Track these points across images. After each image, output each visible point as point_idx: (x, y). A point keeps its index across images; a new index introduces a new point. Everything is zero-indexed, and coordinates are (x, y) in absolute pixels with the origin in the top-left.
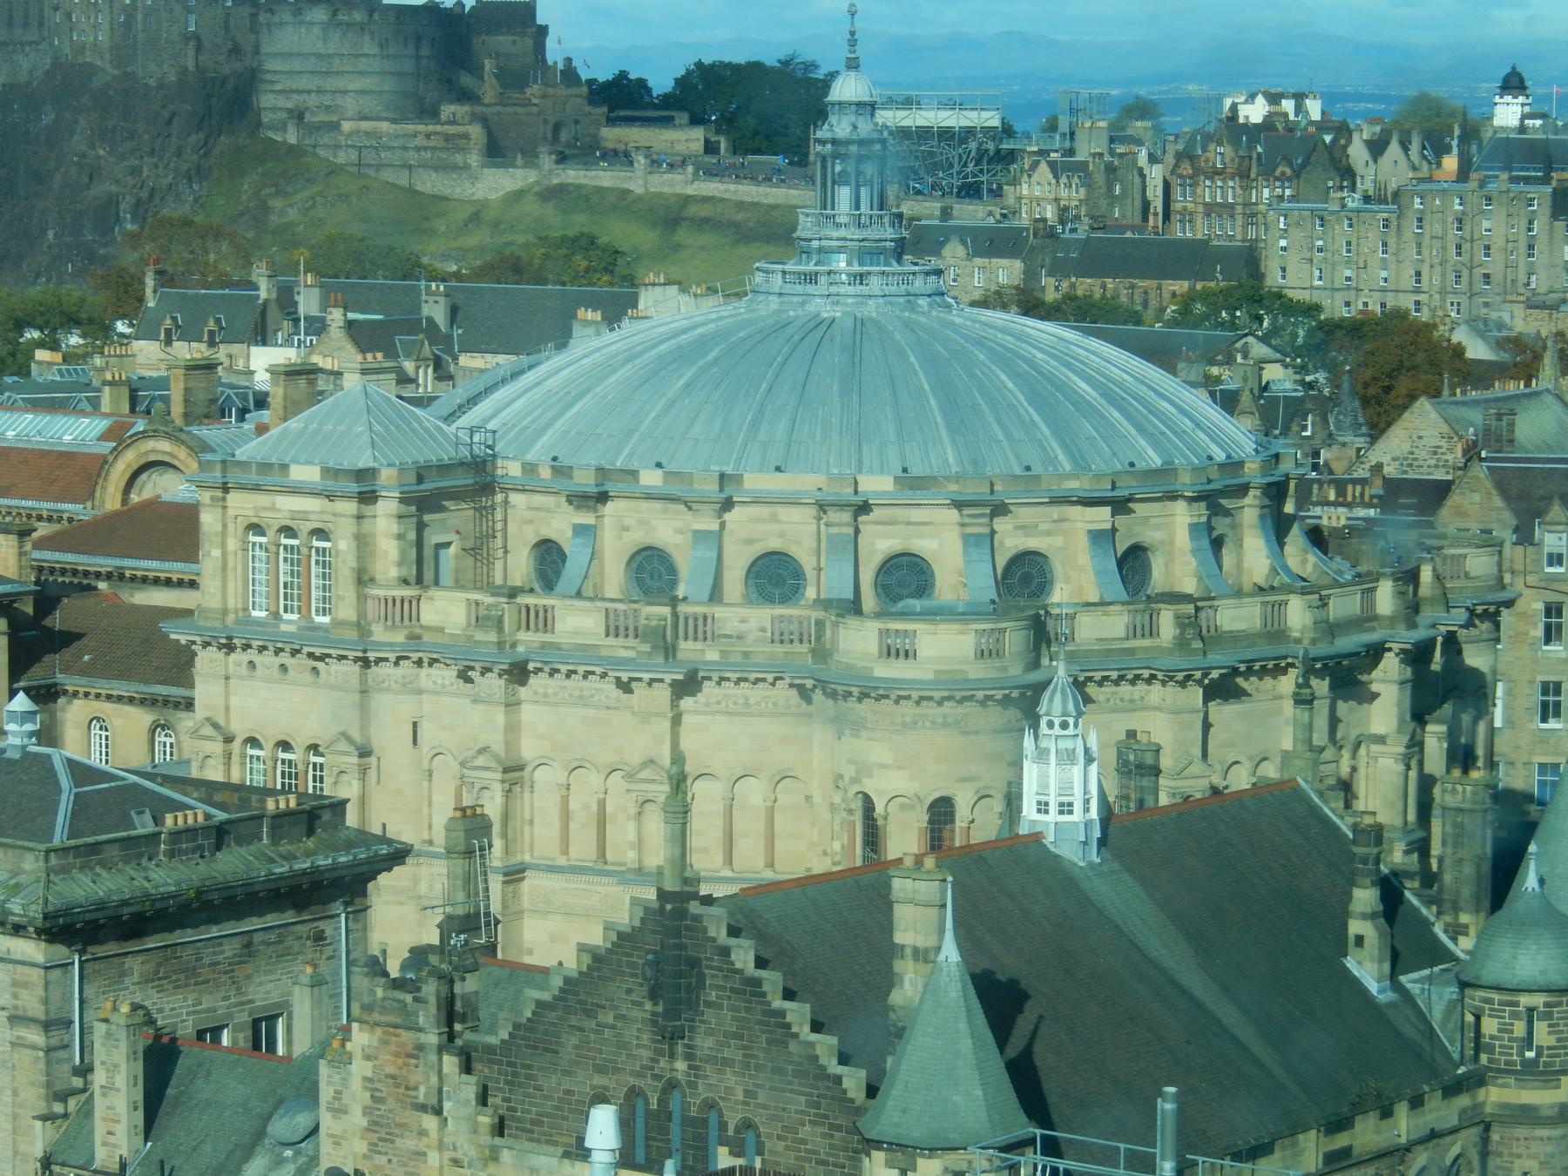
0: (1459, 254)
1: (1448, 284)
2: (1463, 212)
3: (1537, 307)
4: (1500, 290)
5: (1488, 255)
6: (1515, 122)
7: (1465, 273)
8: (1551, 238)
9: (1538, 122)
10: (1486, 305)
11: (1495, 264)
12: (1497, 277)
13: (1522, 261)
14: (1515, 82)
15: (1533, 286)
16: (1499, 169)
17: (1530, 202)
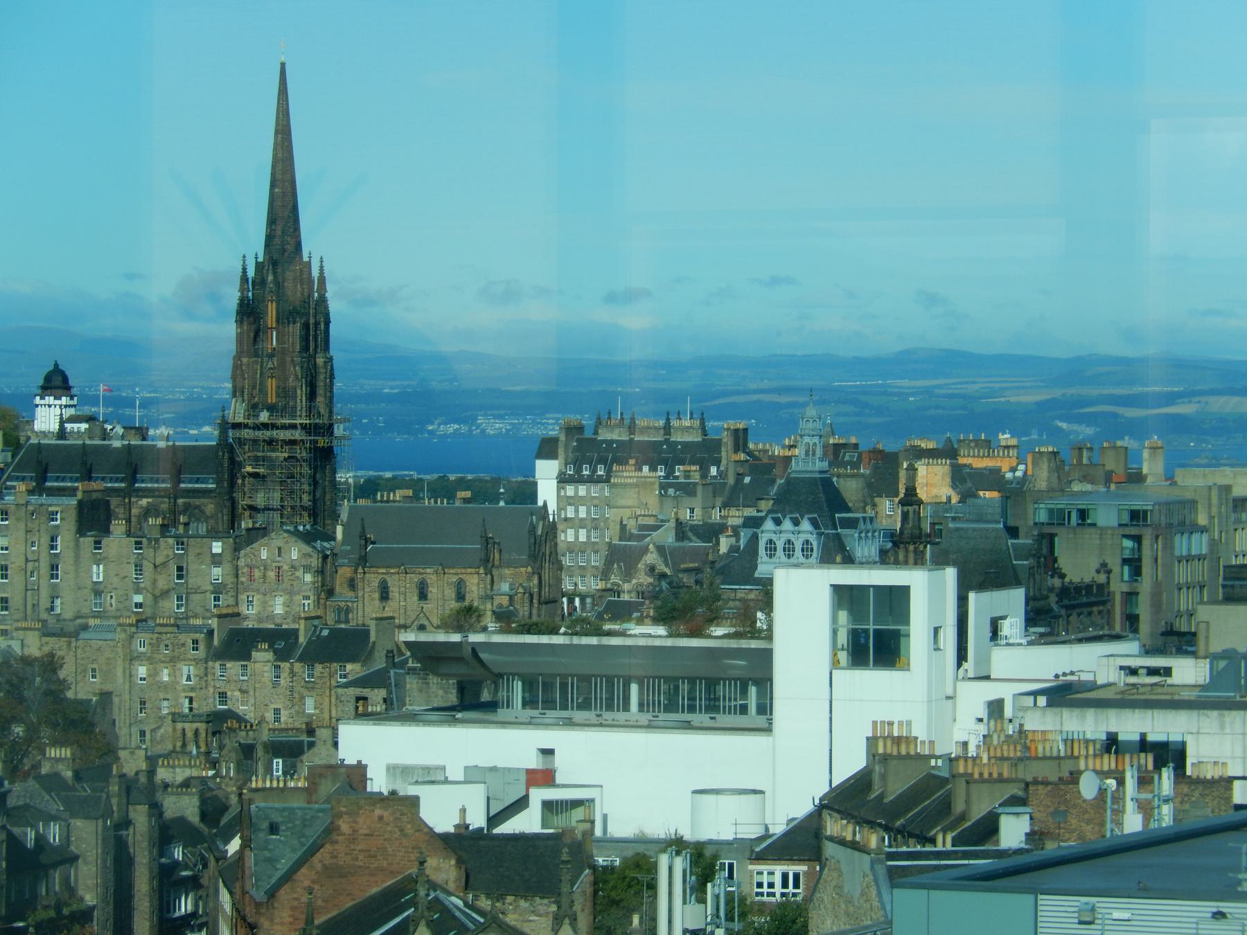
3: (54, 635)
5: (180, 577)
6: (54, 426)
8: (77, 557)
13: (44, 583)
14: (57, 381)
15: (58, 611)
16: (76, 480)
17: (52, 516)
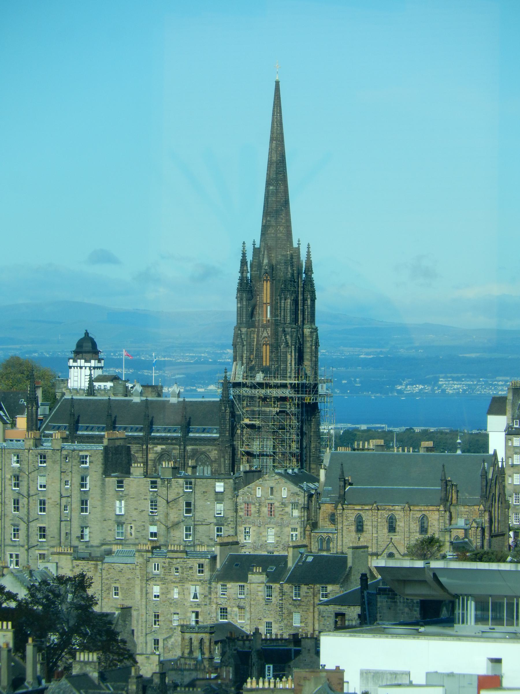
0: (17, 509)
1: (7, 537)
2: (20, 470)
3: (84, 559)
4: (54, 542)
5: (43, 510)
6: (85, 384)
7: (23, 527)
8: (103, 493)
9: (109, 384)
10: (42, 556)
11: (50, 519)
12: (52, 531)
13: (76, 515)
14: (88, 346)
15: (87, 538)
